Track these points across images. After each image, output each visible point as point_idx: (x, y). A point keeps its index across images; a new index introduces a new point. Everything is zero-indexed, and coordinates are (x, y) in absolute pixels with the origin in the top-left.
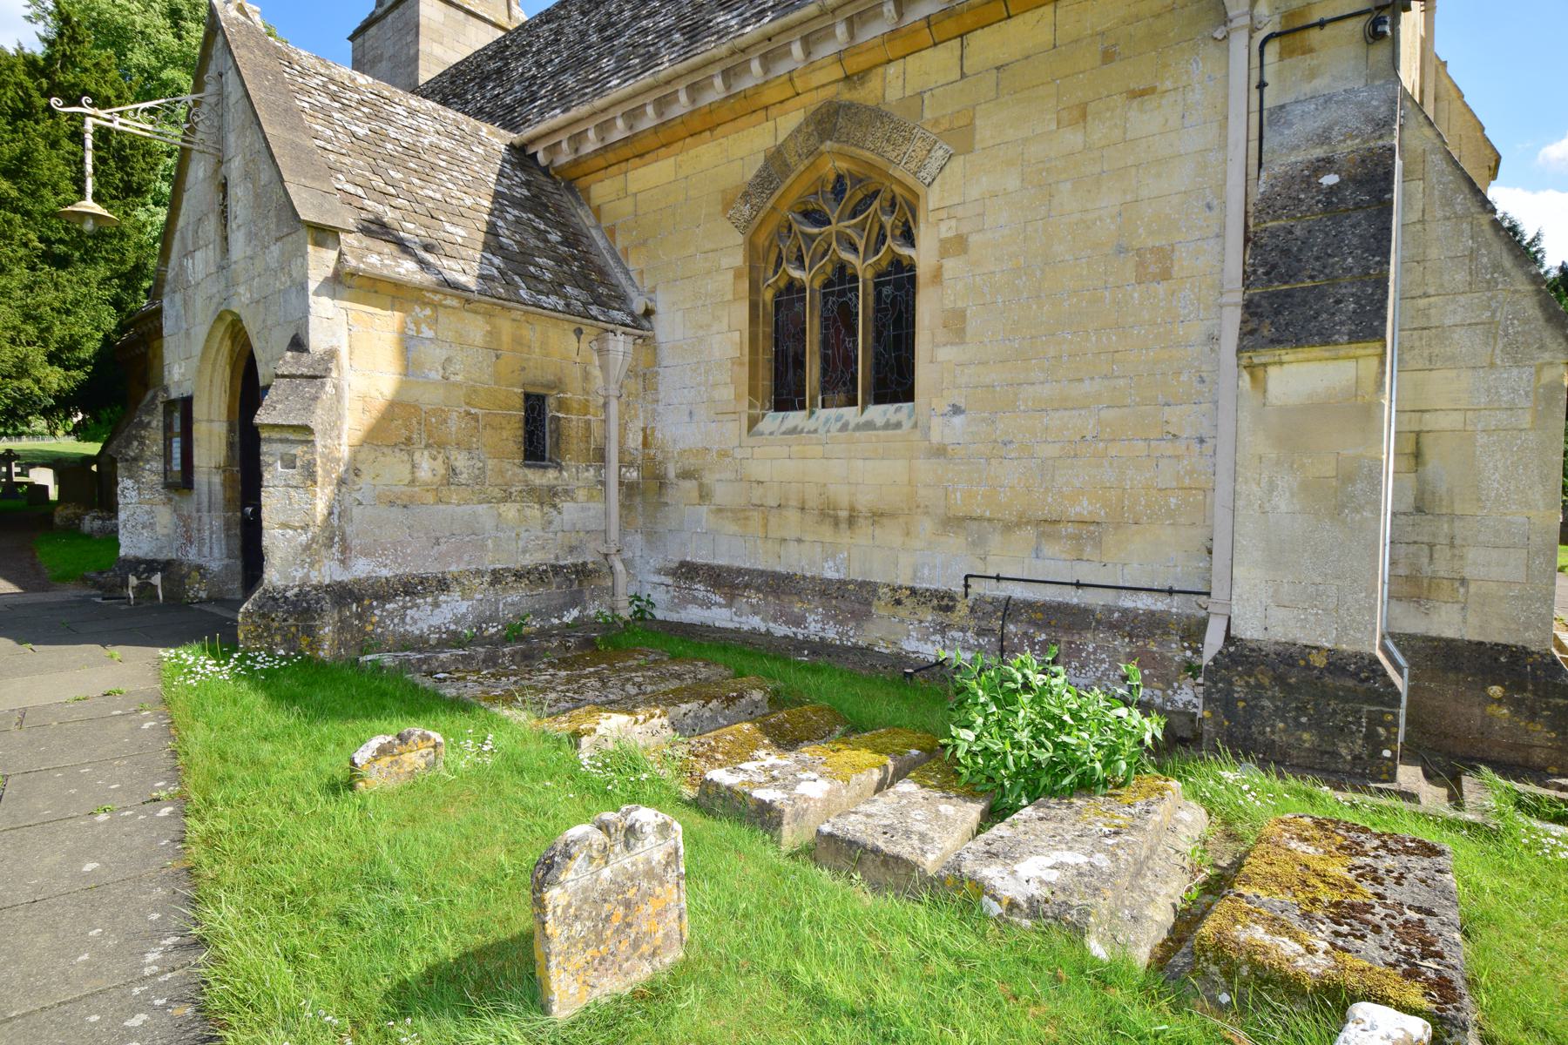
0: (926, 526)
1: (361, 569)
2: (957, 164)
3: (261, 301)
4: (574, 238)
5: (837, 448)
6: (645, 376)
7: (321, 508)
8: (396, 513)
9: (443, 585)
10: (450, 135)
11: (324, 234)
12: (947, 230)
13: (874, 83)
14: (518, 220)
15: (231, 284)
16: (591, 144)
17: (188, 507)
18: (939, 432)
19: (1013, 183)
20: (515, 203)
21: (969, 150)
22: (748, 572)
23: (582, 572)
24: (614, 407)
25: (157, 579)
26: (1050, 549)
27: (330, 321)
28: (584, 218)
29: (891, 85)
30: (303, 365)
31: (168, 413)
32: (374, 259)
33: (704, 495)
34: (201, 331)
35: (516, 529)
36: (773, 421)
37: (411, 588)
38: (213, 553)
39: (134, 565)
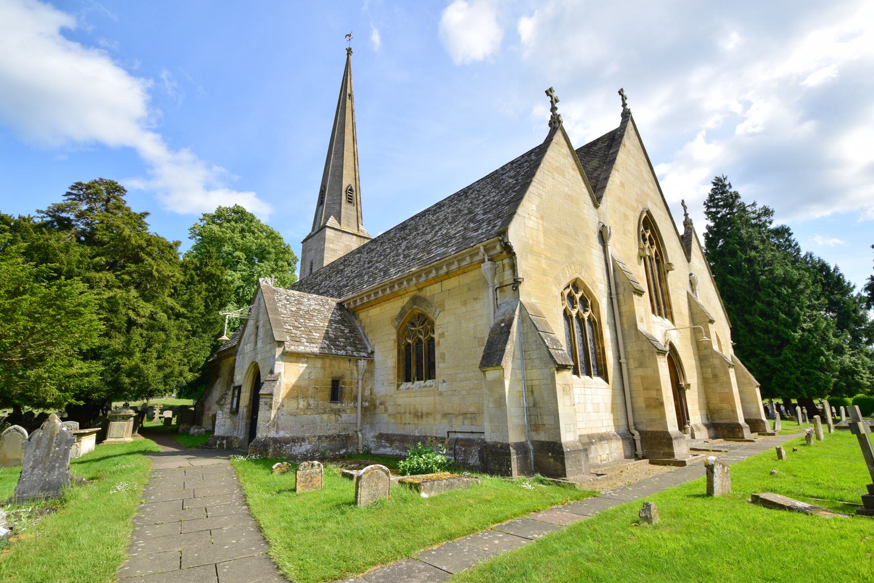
0: (439, 417)
1: (282, 434)
2: (441, 314)
3: (264, 359)
4: (353, 330)
5: (416, 395)
6: (370, 371)
7: (273, 416)
8: (292, 418)
9: (303, 440)
10: (319, 304)
11: (281, 343)
12: (440, 331)
13: (424, 291)
14: (336, 328)
15: (256, 354)
16: (359, 303)
17: (236, 419)
18: (443, 387)
19: (453, 319)
20: (336, 322)
21: (444, 310)
22: (397, 435)
23: (347, 437)
24: (360, 382)
25: (224, 442)
26: (467, 422)
27: (280, 367)
28: (357, 324)
29: (428, 292)
30: (272, 378)
31: (234, 391)
32: (293, 348)
33: (386, 410)
34: (246, 366)
35: (327, 423)
36: (405, 386)
37: (294, 440)
38: (241, 434)
39: (218, 437)
